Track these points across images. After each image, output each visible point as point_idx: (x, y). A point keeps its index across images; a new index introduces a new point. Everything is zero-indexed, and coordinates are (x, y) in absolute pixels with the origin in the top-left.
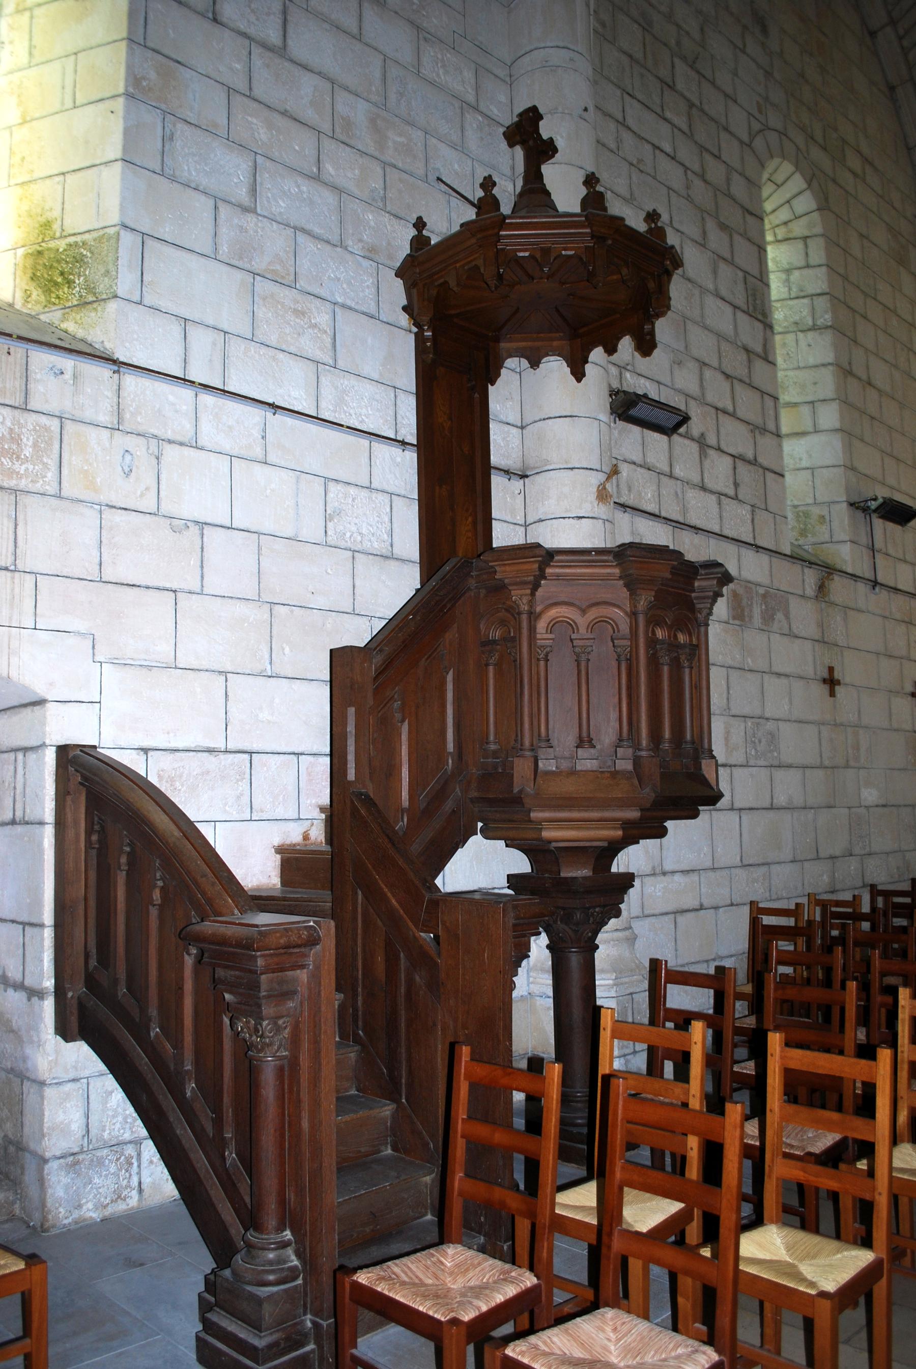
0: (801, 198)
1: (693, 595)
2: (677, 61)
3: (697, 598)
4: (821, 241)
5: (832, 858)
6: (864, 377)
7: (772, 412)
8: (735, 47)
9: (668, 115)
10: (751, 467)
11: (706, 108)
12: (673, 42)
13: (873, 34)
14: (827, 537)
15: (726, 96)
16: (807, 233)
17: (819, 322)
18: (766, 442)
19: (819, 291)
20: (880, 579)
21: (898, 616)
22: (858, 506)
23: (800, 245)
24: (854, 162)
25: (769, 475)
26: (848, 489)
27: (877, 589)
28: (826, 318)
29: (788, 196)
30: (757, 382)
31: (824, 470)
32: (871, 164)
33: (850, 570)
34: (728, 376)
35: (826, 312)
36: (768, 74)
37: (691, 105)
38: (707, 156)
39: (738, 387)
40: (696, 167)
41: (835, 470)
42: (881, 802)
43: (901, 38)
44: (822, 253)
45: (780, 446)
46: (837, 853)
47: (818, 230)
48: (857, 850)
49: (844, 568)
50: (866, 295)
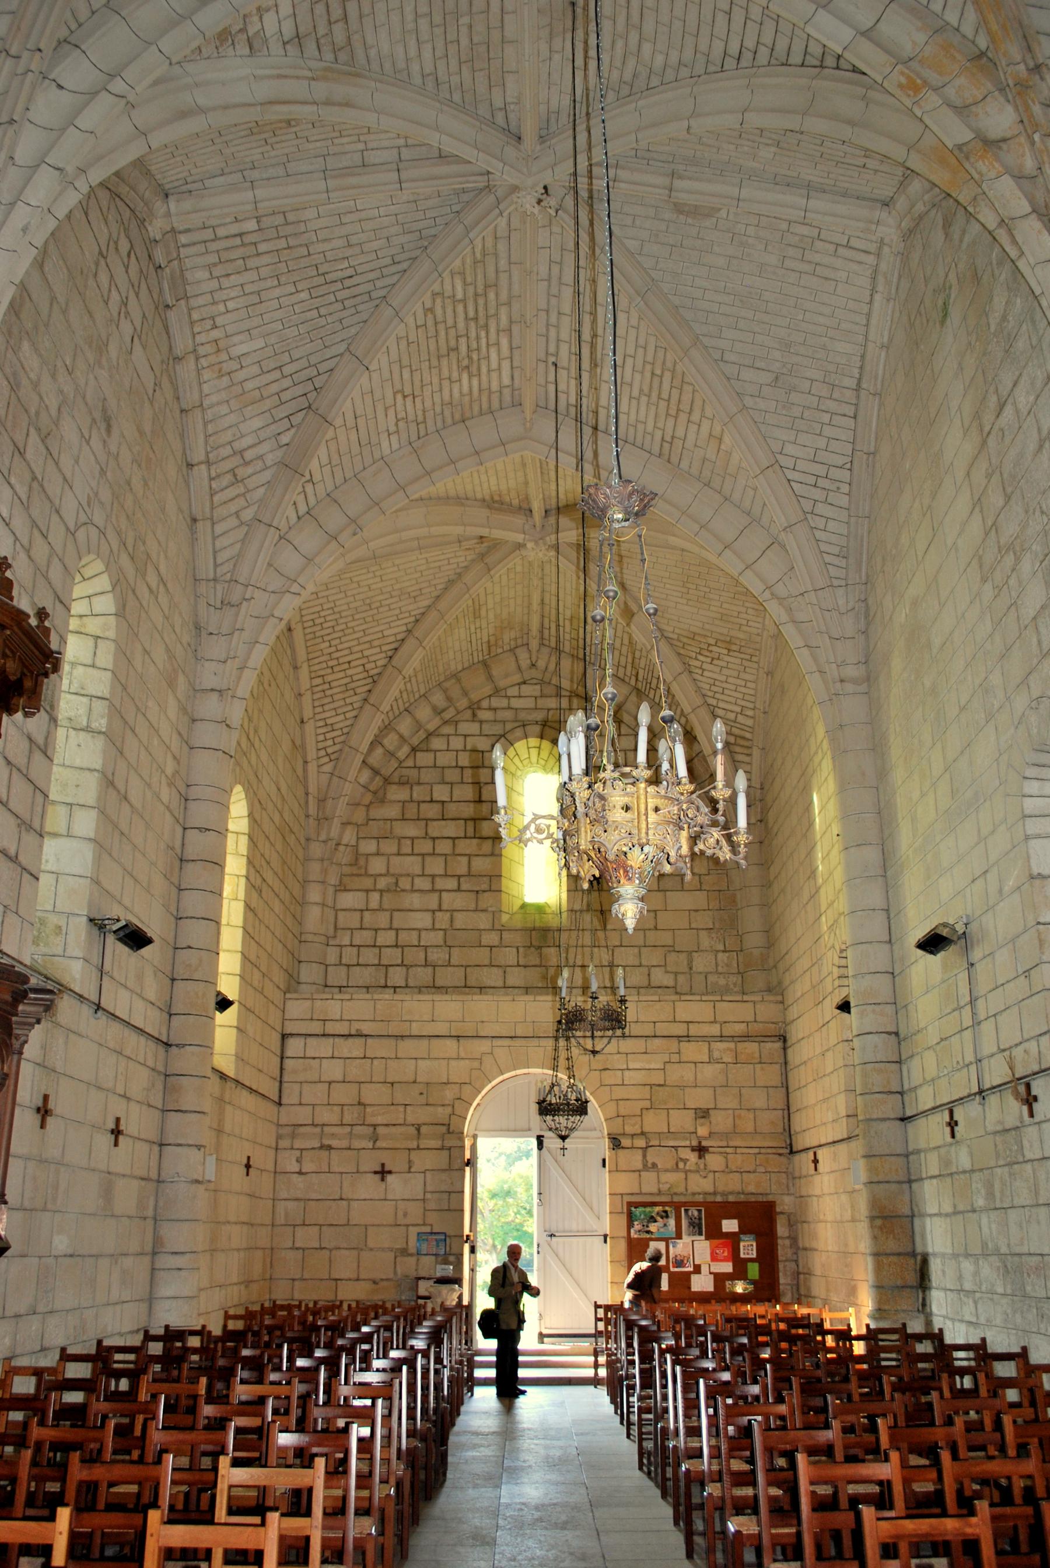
0: (103, 598)
1: (14, 1019)
2: (32, 430)
3: (18, 1023)
4: (112, 646)
5: (17, 1316)
6: (123, 791)
7: (39, 809)
8: (83, 436)
9: (13, 480)
10: (11, 865)
11: (45, 484)
12: (33, 411)
13: (190, 466)
14: (59, 950)
15: (65, 479)
16: (99, 633)
17: (94, 725)
18: (29, 838)
19: (100, 694)
20: (103, 1004)
21: (111, 1045)
22: (98, 924)
23: (91, 642)
24: (152, 579)
25: (26, 875)
26: (90, 904)
27: (100, 1013)
28: (101, 723)
29: (91, 592)
30: (33, 775)
31: (70, 878)
32: (165, 585)
33: (77, 990)
34: (9, 763)
35: (102, 717)
36: (103, 472)
37: (34, 478)
38: (36, 532)
39: (16, 775)
40: (25, 542)
41: (82, 881)
42: (69, 1251)
43: (211, 479)
44: (110, 658)
45: (41, 847)
46: (22, 1312)
47: (111, 634)
48: (41, 1308)
49: (72, 987)
50: (138, 709)
